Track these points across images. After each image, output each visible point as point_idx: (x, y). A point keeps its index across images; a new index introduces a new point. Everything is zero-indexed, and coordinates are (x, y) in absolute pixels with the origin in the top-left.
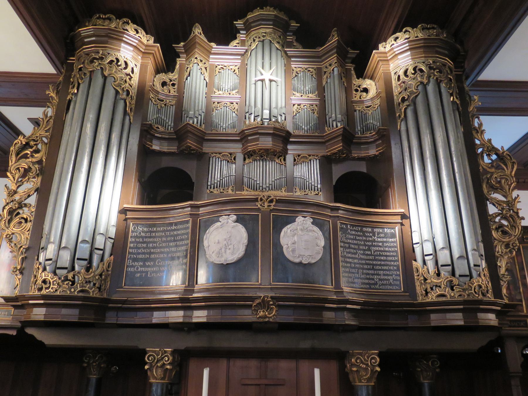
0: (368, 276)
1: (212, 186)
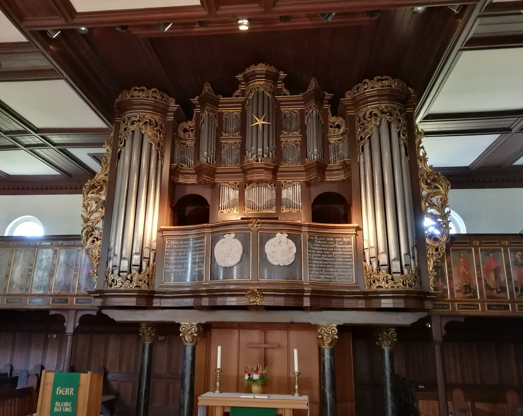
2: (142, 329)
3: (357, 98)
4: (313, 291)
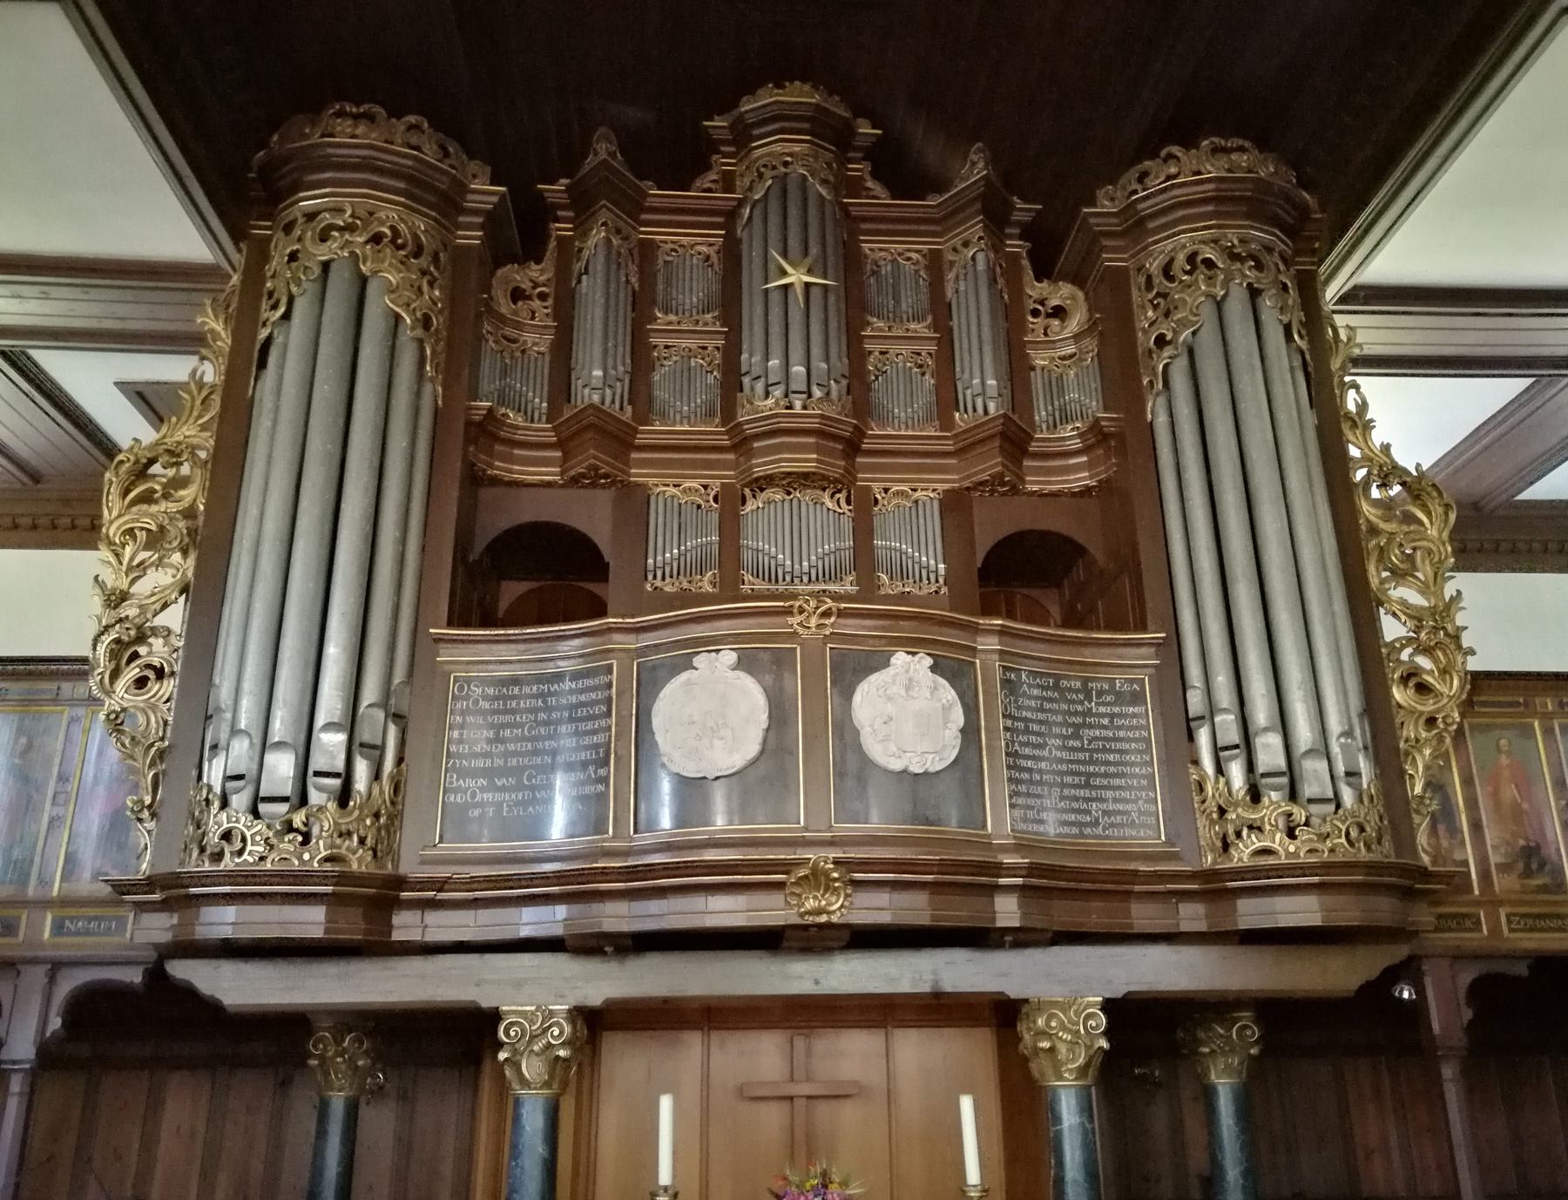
0: (1075, 805)
1: (659, 574)
2: (321, 1040)
3: (1140, 206)
4: (1033, 870)
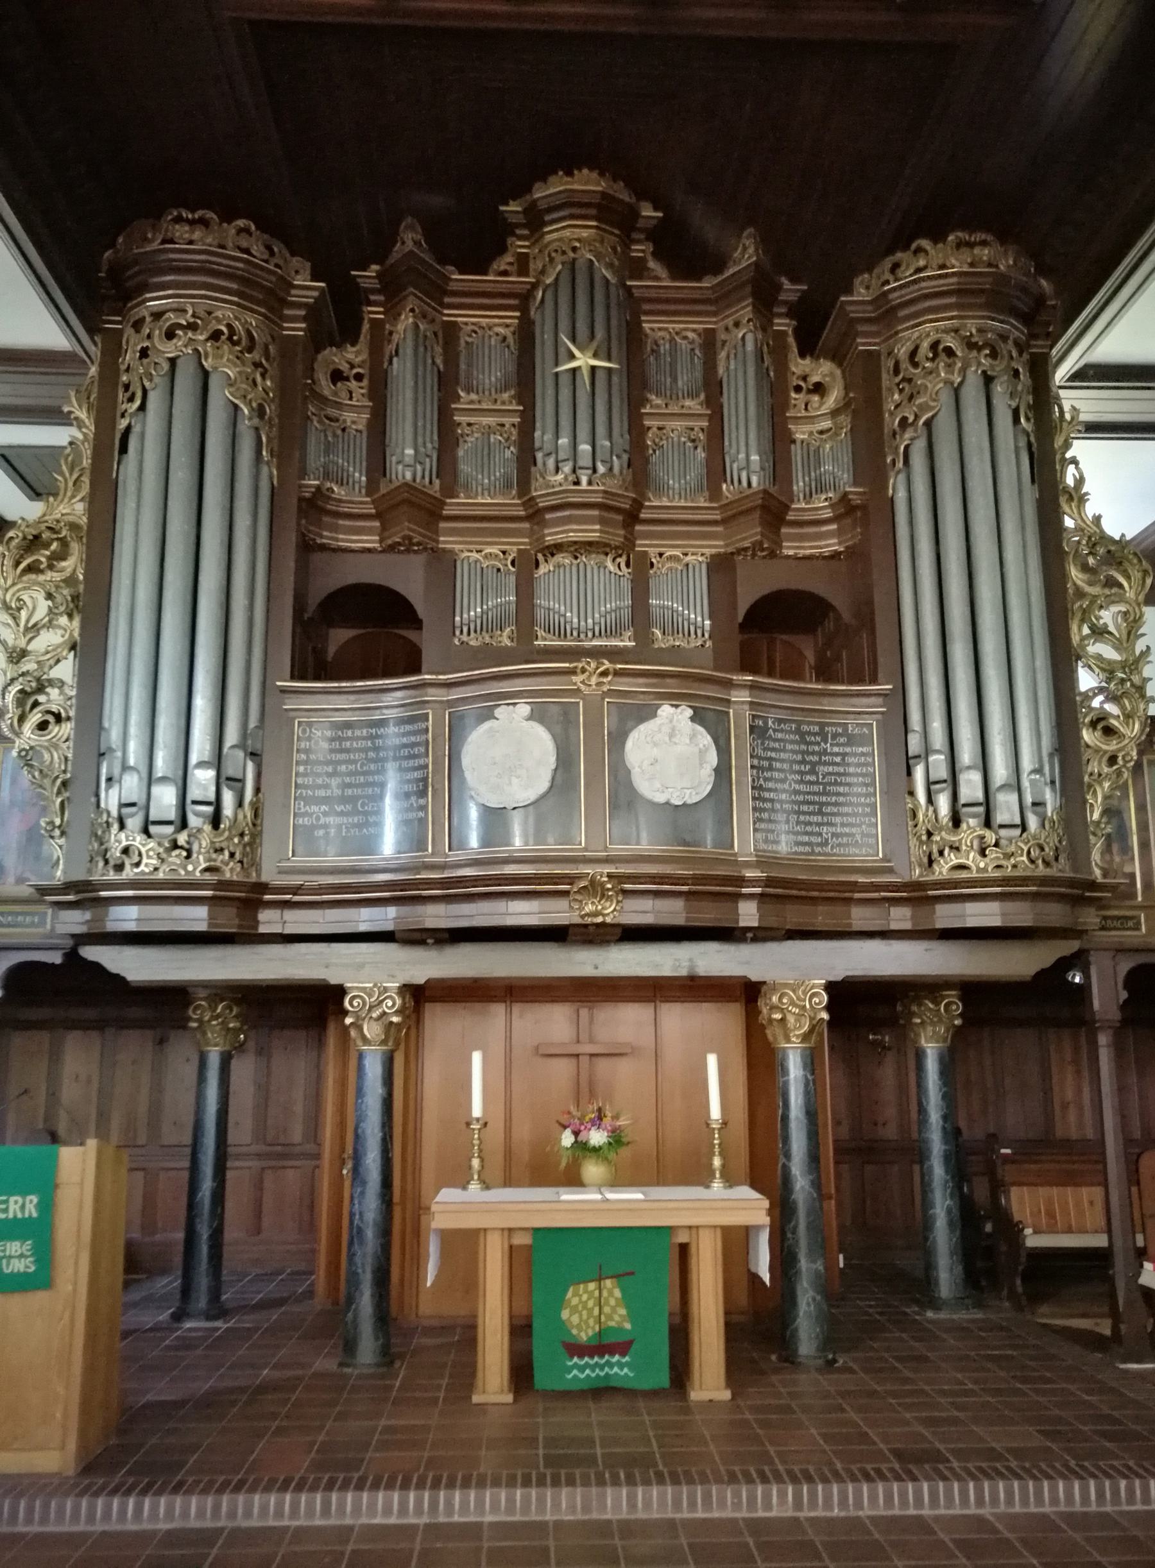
0: (809, 829)
1: (465, 629)
4: (769, 882)
